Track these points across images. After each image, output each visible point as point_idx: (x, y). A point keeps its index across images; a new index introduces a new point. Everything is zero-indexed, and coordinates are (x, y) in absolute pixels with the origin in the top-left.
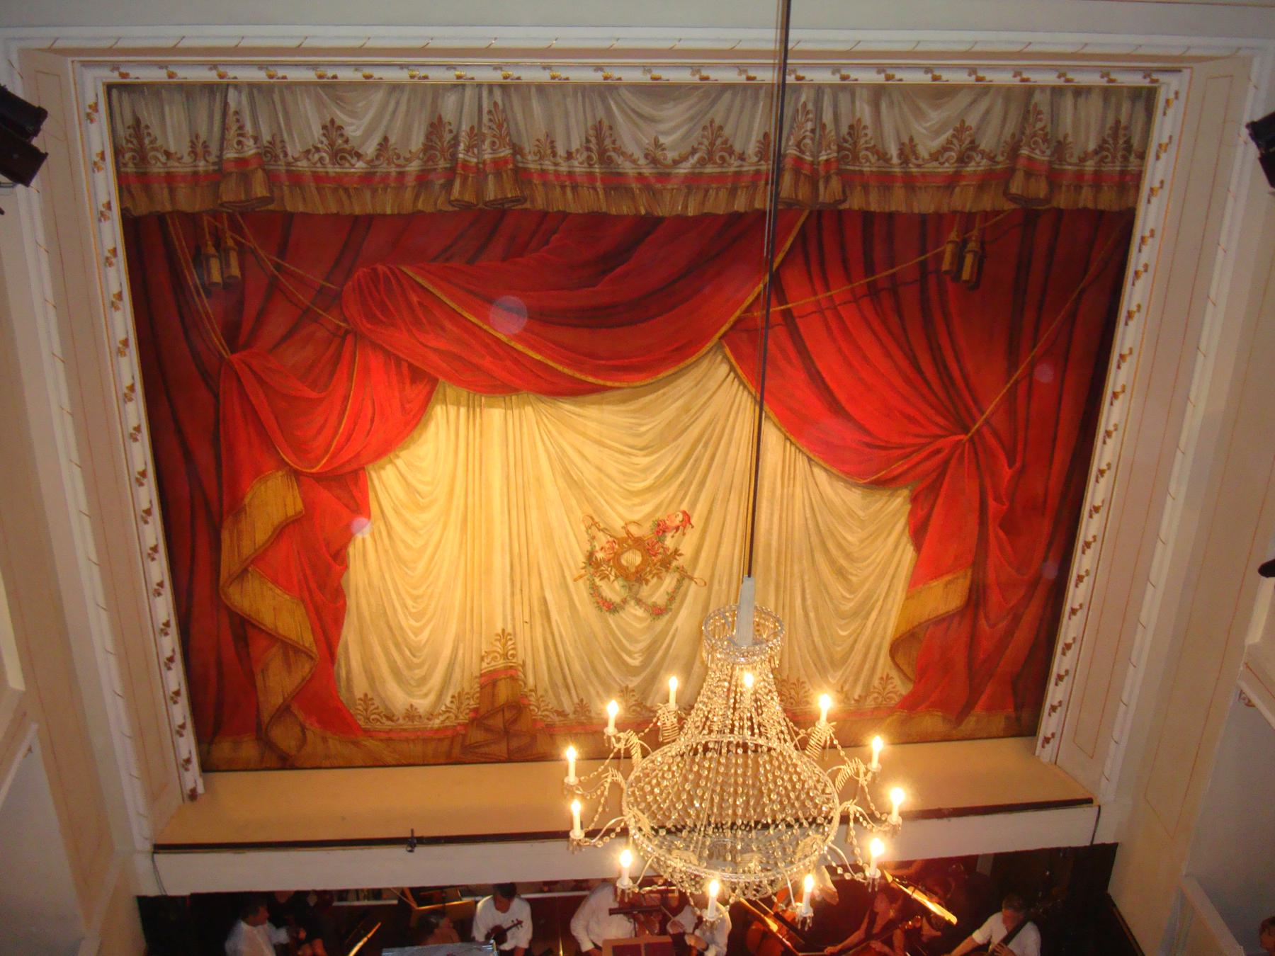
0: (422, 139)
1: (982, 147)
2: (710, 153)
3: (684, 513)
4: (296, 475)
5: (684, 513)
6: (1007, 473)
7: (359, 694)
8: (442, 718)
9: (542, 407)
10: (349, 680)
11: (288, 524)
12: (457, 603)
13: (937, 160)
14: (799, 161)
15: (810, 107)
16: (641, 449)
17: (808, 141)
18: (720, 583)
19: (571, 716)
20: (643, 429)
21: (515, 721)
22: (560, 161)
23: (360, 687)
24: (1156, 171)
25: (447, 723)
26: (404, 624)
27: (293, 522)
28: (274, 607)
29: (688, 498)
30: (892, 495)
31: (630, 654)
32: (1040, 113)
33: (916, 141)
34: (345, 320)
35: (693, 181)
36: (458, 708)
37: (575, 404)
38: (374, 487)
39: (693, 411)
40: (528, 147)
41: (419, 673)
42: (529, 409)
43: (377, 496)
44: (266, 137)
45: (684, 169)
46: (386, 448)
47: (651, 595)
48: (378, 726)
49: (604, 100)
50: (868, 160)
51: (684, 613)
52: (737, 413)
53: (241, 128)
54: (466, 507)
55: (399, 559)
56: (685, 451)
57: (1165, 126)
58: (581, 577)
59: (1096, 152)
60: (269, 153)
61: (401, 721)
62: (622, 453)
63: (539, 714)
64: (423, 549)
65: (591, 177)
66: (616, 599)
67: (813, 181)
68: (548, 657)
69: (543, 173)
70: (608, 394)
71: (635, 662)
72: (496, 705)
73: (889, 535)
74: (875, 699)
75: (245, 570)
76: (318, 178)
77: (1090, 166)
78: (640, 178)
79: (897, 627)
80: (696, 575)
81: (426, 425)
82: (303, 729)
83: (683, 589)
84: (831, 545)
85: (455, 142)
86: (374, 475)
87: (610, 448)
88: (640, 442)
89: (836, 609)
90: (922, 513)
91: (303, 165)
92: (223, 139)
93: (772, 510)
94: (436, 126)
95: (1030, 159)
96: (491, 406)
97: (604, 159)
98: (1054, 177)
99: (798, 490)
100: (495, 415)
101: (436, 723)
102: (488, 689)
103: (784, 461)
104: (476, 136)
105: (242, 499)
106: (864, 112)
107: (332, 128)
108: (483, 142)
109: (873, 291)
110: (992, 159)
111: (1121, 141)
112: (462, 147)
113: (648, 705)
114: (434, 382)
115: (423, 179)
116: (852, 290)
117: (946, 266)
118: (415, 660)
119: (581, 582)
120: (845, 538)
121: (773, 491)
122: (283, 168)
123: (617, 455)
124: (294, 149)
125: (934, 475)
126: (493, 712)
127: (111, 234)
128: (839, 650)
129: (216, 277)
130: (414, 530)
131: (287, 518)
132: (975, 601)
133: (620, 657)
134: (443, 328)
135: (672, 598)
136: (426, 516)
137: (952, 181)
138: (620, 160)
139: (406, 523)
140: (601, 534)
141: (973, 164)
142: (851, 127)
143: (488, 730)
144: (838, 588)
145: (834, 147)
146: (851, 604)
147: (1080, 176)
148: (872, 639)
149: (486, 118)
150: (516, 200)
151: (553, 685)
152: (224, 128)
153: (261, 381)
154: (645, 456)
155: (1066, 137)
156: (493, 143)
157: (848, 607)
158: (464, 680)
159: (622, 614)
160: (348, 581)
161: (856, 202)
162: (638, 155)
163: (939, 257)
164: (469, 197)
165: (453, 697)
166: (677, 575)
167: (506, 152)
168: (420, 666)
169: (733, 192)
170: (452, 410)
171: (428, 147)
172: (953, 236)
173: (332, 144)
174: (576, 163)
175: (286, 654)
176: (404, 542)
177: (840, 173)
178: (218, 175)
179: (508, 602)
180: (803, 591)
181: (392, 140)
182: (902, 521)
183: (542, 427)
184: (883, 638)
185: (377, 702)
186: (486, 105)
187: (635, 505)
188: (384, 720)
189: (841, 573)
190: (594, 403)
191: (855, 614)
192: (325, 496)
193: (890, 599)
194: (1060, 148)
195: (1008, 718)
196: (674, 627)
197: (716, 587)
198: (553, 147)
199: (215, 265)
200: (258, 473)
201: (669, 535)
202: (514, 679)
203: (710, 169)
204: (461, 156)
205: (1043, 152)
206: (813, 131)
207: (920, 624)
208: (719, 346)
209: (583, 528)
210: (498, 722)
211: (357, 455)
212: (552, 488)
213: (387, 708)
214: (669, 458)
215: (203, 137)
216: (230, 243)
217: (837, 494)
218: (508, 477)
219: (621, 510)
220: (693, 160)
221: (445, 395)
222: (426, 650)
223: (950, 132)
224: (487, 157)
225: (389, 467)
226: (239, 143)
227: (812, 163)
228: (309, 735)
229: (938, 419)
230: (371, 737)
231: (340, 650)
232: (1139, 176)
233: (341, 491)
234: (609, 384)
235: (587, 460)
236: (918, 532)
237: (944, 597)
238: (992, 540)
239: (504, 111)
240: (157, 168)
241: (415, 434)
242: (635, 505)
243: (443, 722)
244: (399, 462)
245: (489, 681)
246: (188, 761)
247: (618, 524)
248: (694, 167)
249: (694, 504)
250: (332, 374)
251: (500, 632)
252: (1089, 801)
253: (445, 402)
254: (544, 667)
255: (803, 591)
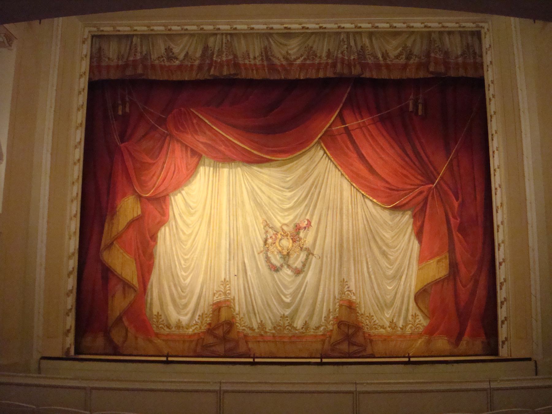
0: (201, 52)
1: (415, 53)
2: (308, 56)
3: (308, 220)
4: (140, 197)
5: (308, 220)
6: (456, 204)
7: (155, 313)
8: (193, 328)
9: (245, 168)
10: (151, 304)
11: (133, 221)
12: (204, 263)
13: (397, 58)
14: (343, 60)
15: (345, 40)
16: (288, 188)
17: (345, 52)
18: (326, 257)
19: (257, 331)
20: (288, 179)
21: (229, 332)
22: (251, 60)
23: (156, 309)
24: (487, 59)
25: (196, 331)
26: (179, 274)
27: (137, 219)
28: (122, 263)
29: (309, 212)
30: (403, 214)
31: (285, 295)
32: (435, 41)
33: (388, 52)
34: (167, 130)
35: (302, 67)
36: (202, 322)
37: (259, 167)
38: (172, 205)
39: (309, 171)
40: (239, 54)
41: (184, 301)
42: (239, 169)
43: (173, 208)
44: (144, 53)
45: (298, 62)
46: (178, 186)
47: (294, 263)
48: (162, 331)
49: (267, 38)
50: (370, 59)
51: (310, 274)
52: (328, 174)
53: (136, 49)
54: (211, 214)
55: (180, 239)
56: (307, 190)
57: (486, 42)
58: (261, 252)
59: (462, 55)
60: (145, 58)
61: (173, 329)
62: (279, 190)
63: (241, 328)
64: (191, 234)
65: (263, 66)
66: (278, 265)
67: (349, 66)
68: (245, 295)
69: (245, 64)
70: (272, 163)
71: (288, 300)
72: (220, 322)
73: (404, 235)
74: (411, 327)
75: (112, 244)
76: (162, 67)
77: (460, 60)
78: (282, 65)
79: (416, 287)
80: (315, 253)
81: (196, 176)
82: (127, 331)
83: (309, 260)
84: (378, 239)
85: (213, 54)
86: (172, 198)
87: (274, 188)
88: (287, 185)
89: (384, 273)
90: (419, 224)
91: (157, 62)
92: (129, 53)
93: (348, 219)
94: (206, 48)
95: (435, 58)
96: (223, 167)
97: (268, 59)
98: (446, 64)
99: (359, 210)
100: (225, 171)
101: (190, 331)
102: (216, 313)
103: (351, 195)
104: (220, 52)
105: (116, 208)
106: (367, 41)
107: (168, 50)
108: (223, 54)
109: (382, 120)
110: (420, 58)
111: (471, 51)
112: (215, 56)
113: (295, 326)
114: (200, 156)
115: (200, 67)
116: (373, 119)
117: (411, 109)
118: (183, 294)
119: (261, 254)
120: (384, 236)
121: (348, 210)
122: (149, 64)
123: (277, 191)
124: (154, 56)
125: (422, 204)
126: (217, 327)
127: (84, 83)
128: (389, 298)
129: (120, 113)
130: (188, 225)
131: (134, 218)
132: (453, 267)
133: (280, 297)
134: (205, 133)
135: (304, 265)
136: (193, 218)
137: (405, 67)
138: (274, 59)
139: (184, 222)
140: (270, 230)
141: (412, 60)
142: (362, 47)
143: (215, 336)
144: (384, 263)
145: (356, 54)
146: (392, 272)
147: (457, 64)
148: (404, 292)
149: (224, 45)
150: (235, 74)
151: (248, 312)
152: (130, 49)
153: (130, 154)
154: (290, 192)
155: (448, 49)
156: (227, 54)
157: (390, 273)
158: (205, 307)
159: (281, 273)
160: (156, 251)
161: (367, 75)
162: (281, 57)
163: (407, 106)
164: (217, 74)
165: (199, 316)
166: (306, 253)
167: (231, 57)
168: (185, 297)
169: (318, 70)
170: (207, 168)
171: (203, 55)
172: (412, 97)
173: (168, 55)
174: (257, 61)
175: (124, 288)
176: (182, 231)
177: (359, 63)
178: (126, 66)
179: (228, 264)
180: (367, 263)
181: (190, 53)
182: (410, 227)
183: (245, 177)
184: (410, 291)
185: (163, 317)
186: (224, 41)
187: (286, 216)
188: (165, 328)
189: (384, 254)
190: (267, 167)
191: (394, 277)
192: (150, 207)
193: (411, 269)
194: (446, 53)
195: (483, 342)
196: (306, 281)
197: (325, 259)
198: (248, 55)
199: (120, 108)
200: (124, 195)
201: (302, 231)
202: (229, 307)
203: (308, 62)
204: (214, 59)
205: (440, 55)
206: (347, 48)
207: (428, 284)
208: (318, 143)
209: (262, 227)
210: (220, 332)
211: (166, 189)
212: (249, 206)
213: (167, 321)
214: (300, 192)
215: (122, 53)
216: (127, 99)
217: (378, 212)
218: (229, 201)
219: (279, 218)
220: (302, 59)
221: (204, 162)
222: (188, 289)
223: (400, 49)
224: (224, 59)
225: (179, 195)
226: (135, 55)
227: (348, 60)
228: (129, 335)
229: (419, 177)
230: (158, 338)
231: (149, 287)
232: (482, 65)
233: (157, 205)
234: (273, 158)
235: (264, 193)
236: (419, 234)
237: (437, 269)
238: (456, 238)
239: (231, 42)
240: (104, 64)
241: (191, 179)
242: (286, 216)
243: (193, 330)
244: (183, 192)
245: (217, 308)
246: (69, 331)
247: (278, 225)
248: (302, 61)
249: (312, 215)
250: (159, 153)
251: (223, 280)
252: (529, 359)
253: (204, 165)
254: (244, 301)
255: (367, 263)
